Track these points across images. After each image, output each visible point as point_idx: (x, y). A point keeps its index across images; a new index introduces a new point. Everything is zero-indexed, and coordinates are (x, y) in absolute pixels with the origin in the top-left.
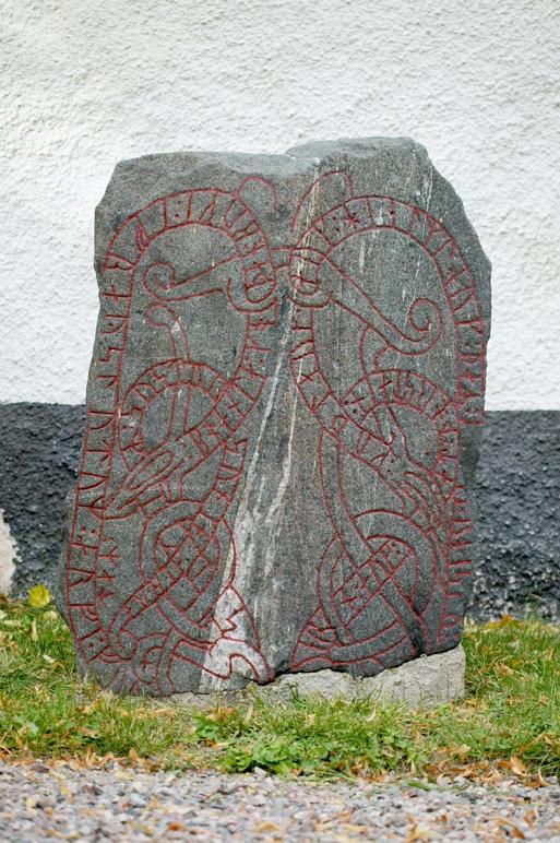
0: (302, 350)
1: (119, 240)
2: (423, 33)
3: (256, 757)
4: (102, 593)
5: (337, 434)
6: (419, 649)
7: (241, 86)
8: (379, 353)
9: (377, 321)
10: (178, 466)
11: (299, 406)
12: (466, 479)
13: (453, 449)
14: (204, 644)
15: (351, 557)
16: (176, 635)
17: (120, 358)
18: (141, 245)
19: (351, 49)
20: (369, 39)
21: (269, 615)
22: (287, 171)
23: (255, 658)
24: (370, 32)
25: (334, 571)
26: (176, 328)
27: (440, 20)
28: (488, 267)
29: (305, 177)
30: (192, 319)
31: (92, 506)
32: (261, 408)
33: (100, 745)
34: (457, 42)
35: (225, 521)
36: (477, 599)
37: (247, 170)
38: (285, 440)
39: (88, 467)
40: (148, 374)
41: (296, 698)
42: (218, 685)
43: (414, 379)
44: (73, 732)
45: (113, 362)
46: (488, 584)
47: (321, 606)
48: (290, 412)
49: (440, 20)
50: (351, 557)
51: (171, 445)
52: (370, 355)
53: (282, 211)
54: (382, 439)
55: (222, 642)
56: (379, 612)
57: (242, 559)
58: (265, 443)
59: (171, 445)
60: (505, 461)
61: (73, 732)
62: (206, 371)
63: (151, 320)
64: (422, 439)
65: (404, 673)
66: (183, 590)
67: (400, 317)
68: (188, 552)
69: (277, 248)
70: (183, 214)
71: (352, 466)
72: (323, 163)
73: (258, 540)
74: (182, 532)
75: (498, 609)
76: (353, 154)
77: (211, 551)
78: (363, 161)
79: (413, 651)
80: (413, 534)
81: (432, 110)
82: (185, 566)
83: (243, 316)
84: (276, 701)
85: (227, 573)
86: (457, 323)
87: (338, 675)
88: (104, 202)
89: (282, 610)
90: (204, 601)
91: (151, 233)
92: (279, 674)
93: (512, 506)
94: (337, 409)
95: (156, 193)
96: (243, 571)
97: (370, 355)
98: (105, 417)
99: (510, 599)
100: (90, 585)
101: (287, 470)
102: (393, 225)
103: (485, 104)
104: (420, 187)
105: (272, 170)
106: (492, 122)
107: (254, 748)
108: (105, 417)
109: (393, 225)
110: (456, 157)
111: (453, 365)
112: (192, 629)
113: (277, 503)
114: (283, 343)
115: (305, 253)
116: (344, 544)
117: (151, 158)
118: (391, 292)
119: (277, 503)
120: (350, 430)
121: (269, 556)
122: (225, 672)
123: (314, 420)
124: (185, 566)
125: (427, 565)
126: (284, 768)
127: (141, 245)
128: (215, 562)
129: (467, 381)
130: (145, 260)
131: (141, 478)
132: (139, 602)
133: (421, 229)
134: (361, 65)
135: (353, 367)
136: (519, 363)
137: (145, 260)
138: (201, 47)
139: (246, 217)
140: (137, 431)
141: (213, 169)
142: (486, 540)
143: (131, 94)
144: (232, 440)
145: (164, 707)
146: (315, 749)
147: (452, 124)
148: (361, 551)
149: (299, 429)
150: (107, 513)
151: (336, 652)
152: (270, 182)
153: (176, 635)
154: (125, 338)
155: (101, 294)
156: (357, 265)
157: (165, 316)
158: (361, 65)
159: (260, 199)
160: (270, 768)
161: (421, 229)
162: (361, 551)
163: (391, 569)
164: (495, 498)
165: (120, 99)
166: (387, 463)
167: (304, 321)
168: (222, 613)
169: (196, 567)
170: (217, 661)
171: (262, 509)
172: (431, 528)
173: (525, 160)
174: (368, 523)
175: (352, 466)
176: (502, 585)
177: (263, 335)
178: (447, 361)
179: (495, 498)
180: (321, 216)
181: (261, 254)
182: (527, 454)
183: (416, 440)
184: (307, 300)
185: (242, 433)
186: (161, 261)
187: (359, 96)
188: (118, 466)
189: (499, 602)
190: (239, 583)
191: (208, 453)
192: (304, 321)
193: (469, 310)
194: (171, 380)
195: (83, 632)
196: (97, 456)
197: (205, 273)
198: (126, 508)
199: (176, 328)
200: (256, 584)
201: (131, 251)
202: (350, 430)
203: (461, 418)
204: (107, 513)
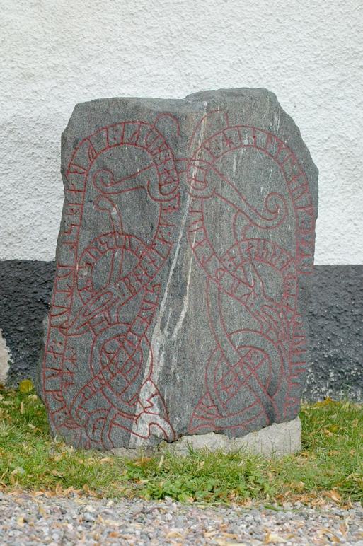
0: (196, 226)
4: (69, 384)
5: (218, 280)
6: (271, 419)
9: (244, 208)
11: (194, 262)
13: (293, 290)
14: (133, 417)
18: (93, 158)
20: (239, 24)
25: (216, 369)
26: (114, 212)
32: (170, 263)
33: (66, 482)
35: (145, 336)
39: (58, 302)
42: (140, 442)
43: (269, 246)
46: (317, 377)
47: (208, 392)
50: (227, 360)
56: (246, 396)
64: (273, 286)
65: (263, 434)
71: (230, 303)
73: (167, 349)
74: (118, 344)
75: (324, 393)
80: (268, 346)
81: (280, 70)
83: (157, 204)
85: (147, 370)
86: (296, 208)
93: (331, 326)
94: (218, 264)
96: (158, 370)
97: (240, 229)
99: (331, 387)
101: (186, 304)
103: (314, 66)
109: (255, 145)
111: (293, 236)
115: (197, 163)
122: (147, 434)
125: (277, 366)
128: (141, 364)
129: (302, 246)
133: (273, 148)
136: (336, 234)
137: (94, 167)
138: (129, 29)
139: (160, 140)
143: (84, 60)
148: (233, 356)
149: (194, 277)
150: (70, 332)
153: (114, 411)
154: (81, 218)
156: (231, 170)
162: (233, 356)
163: (254, 369)
164: (321, 322)
165: (77, 63)
168: (144, 396)
170: (142, 428)
171: (171, 330)
174: (239, 339)
175: (230, 303)
176: (326, 377)
179: (321, 322)
180: (207, 139)
183: (270, 284)
184: (199, 193)
185: (157, 280)
186: (105, 169)
187: (232, 61)
188: (77, 301)
189: (324, 389)
192: (197, 207)
196: (62, 295)
201: (85, 162)
202: (227, 280)
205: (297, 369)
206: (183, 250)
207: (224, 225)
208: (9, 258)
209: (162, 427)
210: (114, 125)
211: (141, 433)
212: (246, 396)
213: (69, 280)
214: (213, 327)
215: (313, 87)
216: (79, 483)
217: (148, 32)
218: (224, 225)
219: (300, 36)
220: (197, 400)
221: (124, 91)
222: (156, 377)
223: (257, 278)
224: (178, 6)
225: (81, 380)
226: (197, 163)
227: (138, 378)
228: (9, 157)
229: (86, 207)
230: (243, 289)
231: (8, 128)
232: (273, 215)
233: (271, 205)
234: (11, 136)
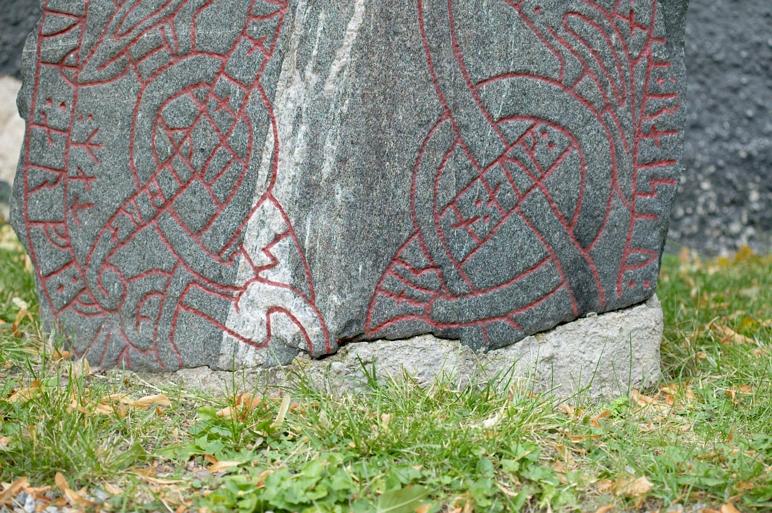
4: (76, 204)
6: (584, 304)
14: (228, 290)
16: (183, 275)
23: (305, 315)
31: (61, 62)
36: (703, 222)
41: (372, 381)
42: (250, 357)
46: (720, 201)
47: (417, 231)
50: (470, 150)
56: (517, 241)
57: (287, 150)
66: (195, 201)
73: (313, 118)
75: (736, 236)
79: (575, 307)
80: (578, 114)
84: (336, 380)
85: (263, 172)
90: (226, 221)
92: (343, 342)
96: (288, 170)
99: (751, 223)
100: (58, 190)
112: (208, 264)
116: (457, 128)
119: (344, 57)
121: (330, 147)
125: (600, 168)
128: (246, 155)
132: (127, 221)
142: (717, 138)
145: (158, 392)
148: (488, 141)
150: (84, 75)
151: (442, 307)
153: (183, 275)
162: (488, 141)
168: (255, 238)
169: (214, 163)
170: (246, 318)
171: (321, 68)
176: (740, 202)
179: (732, 78)
189: (735, 228)
190: (284, 190)
195: (48, 265)
200: (310, 192)
204: (84, 75)
209: (303, 320)
222: (284, 190)
225: (111, 196)
227: (239, 193)
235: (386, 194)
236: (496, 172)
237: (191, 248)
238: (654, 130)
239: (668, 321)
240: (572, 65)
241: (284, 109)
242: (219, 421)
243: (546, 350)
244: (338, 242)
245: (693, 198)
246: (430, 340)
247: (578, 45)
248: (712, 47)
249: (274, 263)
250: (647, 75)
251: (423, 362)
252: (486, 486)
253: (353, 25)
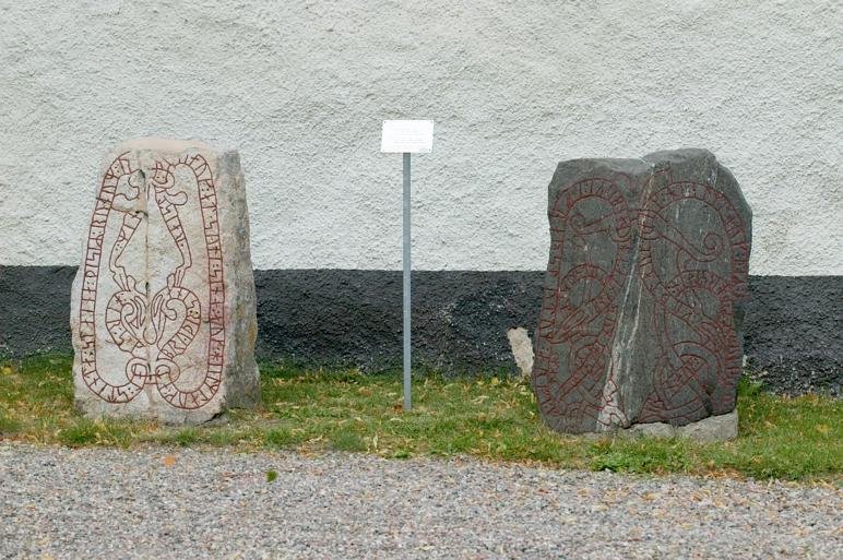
0: (645, 262)
1: (560, 202)
2: (761, 61)
3: (607, 464)
4: (551, 381)
5: (664, 303)
6: (710, 413)
7: (658, 94)
8: (687, 262)
9: (685, 245)
10: (586, 318)
11: (643, 290)
12: (737, 326)
13: (729, 310)
14: (599, 408)
15: (672, 366)
16: (585, 403)
17: (560, 263)
18: (570, 206)
19: (720, 72)
20: (729, 66)
21: (628, 394)
22: (637, 171)
23: (622, 416)
24: (730, 62)
25: (662, 372)
26: (586, 248)
27: (771, 54)
28: (750, 215)
29: (647, 174)
30: (593, 244)
31: (547, 337)
32: (625, 290)
33: (535, 456)
34: (781, 67)
35: (608, 347)
36: (793, 383)
37: (620, 169)
38: (635, 307)
39: (546, 317)
40: (573, 272)
41: (642, 435)
42: (605, 429)
43: (707, 275)
44: (524, 450)
45: (556, 264)
46: (800, 375)
47: (655, 390)
48: (638, 293)
49: (771, 54)
50: (672, 366)
51: (583, 307)
52: (682, 263)
53: (635, 192)
54: (689, 306)
55: (607, 407)
56: (687, 393)
57: (615, 364)
58: (626, 308)
59: (583, 307)
60: (811, 305)
61: (524, 450)
62: (599, 271)
63: (574, 244)
64: (712, 305)
65: (702, 425)
66: (588, 381)
67: (698, 243)
68: (591, 362)
69: (631, 211)
70: (589, 191)
71: (673, 321)
72: (656, 167)
73: (623, 356)
74: (588, 352)
75: (806, 389)
76: (673, 161)
77: (602, 361)
78: (677, 164)
79: (706, 414)
80: (706, 353)
81: (767, 105)
82: (589, 368)
83: (616, 244)
84: (631, 436)
85: (609, 372)
86: (732, 244)
87: (664, 425)
88: (552, 183)
89: (634, 392)
90: (598, 388)
91: (579, 195)
92: (633, 424)
93: (814, 331)
94: (664, 290)
95: (576, 179)
96: (616, 372)
97: (682, 263)
98: (553, 292)
99: (812, 384)
100: (545, 377)
101: (637, 322)
102: (695, 196)
103: (798, 101)
104: (710, 176)
105: (631, 169)
106: (802, 112)
107: (609, 460)
108: (553, 292)
109: (695, 196)
110: (781, 132)
111: (729, 268)
112: (593, 400)
113: (632, 339)
114: (635, 258)
115: (646, 213)
116: (668, 359)
117: (574, 161)
118: (694, 231)
119: (632, 339)
120: (671, 302)
121: (628, 365)
122: (608, 422)
123: (651, 297)
124: (589, 368)
125: (714, 369)
126: (620, 469)
127: (570, 206)
128: (603, 367)
129: (737, 275)
130: (571, 213)
131: (569, 323)
132: (569, 386)
133: (710, 198)
134: (725, 81)
135: (672, 269)
136: (819, 249)
137: (571, 213)
138: (635, 72)
139: (617, 195)
140: (568, 300)
141: (603, 169)
142: (798, 350)
143: (595, 100)
144: (611, 306)
145: (577, 439)
146: (638, 460)
147: (779, 114)
148: (677, 362)
149: (642, 301)
150: (554, 341)
151: (663, 413)
152: (629, 176)
153: (585, 403)
154: (562, 252)
155: (551, 230)
156: (674, 218)
157: (580, 242)
158: (725, 81)
159: (622, 184)
160: (613, 469)
161: (710, 198)
162: (677, 362)
163: (694, 372)
164: (805, 326)
165: (589, 103)
166: (692, 318)
167: (645, 247)
168: (607, 392)
169: (595, 369)
170: (604, 417)
171: (626, 341)
172: (717, 351)
173: (822, 133)
174: (681, 349)
175: (673, 321)
176: (808, 375)
177: (625, 254)
178: (726, 265)
179: (805, 326)
180: (654, 194)
181: (624, 213)
182: (824, 301)
183: (708, 306)
184: (647, 236)
185: (615, 302)
186: (579, 214)
187: (724, 98)
188: (559, 317)
189: (806, 386)
190: (615, 378)
191: (600, 312)
192: (645, 247)
193: (739, 237)
194: (583, 274)
195: (542, 400)
196: (549, 312)
197: (598, 221)
198: (563, 339)
199: (586, 248)
200: (623, 379)
201: (565, 208)
202: (671, 302)
203: (733, 293)
204: (554, 341)
205: (732, 373)
206: (635, 280)
207: (668, 260)
208: (533, 270)
209: (620, 417)
210: (585, 180)
211: (604, 421)
212: (687, 393)
213: (552, 301)
214: (660, 340)
215: (796, 120)
216: (544, 457)
217: (650, 75)
218: (668, 260)
219: (785, 75)
220: (646, 397)
221: (436, 255)
222: (615, 378)
223: (696, 300)
224: (675, 52)
225: (562, 378)
226: (646, 213)
227: (601, 378)
228: (533, 183)
229: (565, 244)
230: (684, 310)
231: (532, 159)
232: (711, 252)
233: (710, 243)
234: (534, 166)
235: (645, 379)
236: (680, 372)
237: (588, 396)
238: (731, 358)
239: (740, 419)
240: (705, 339)
241: (615, 354)
242: (596, 447)
243: (697, 427)
244: (631, 394)
245: (789, 374)
246: (659, 423)
247: (706, 333)
248: (796, 314)
249: (612, 400)
250: (729, 340)
251: (656, 430)
252: (668, 463)
253: (635, 329)
